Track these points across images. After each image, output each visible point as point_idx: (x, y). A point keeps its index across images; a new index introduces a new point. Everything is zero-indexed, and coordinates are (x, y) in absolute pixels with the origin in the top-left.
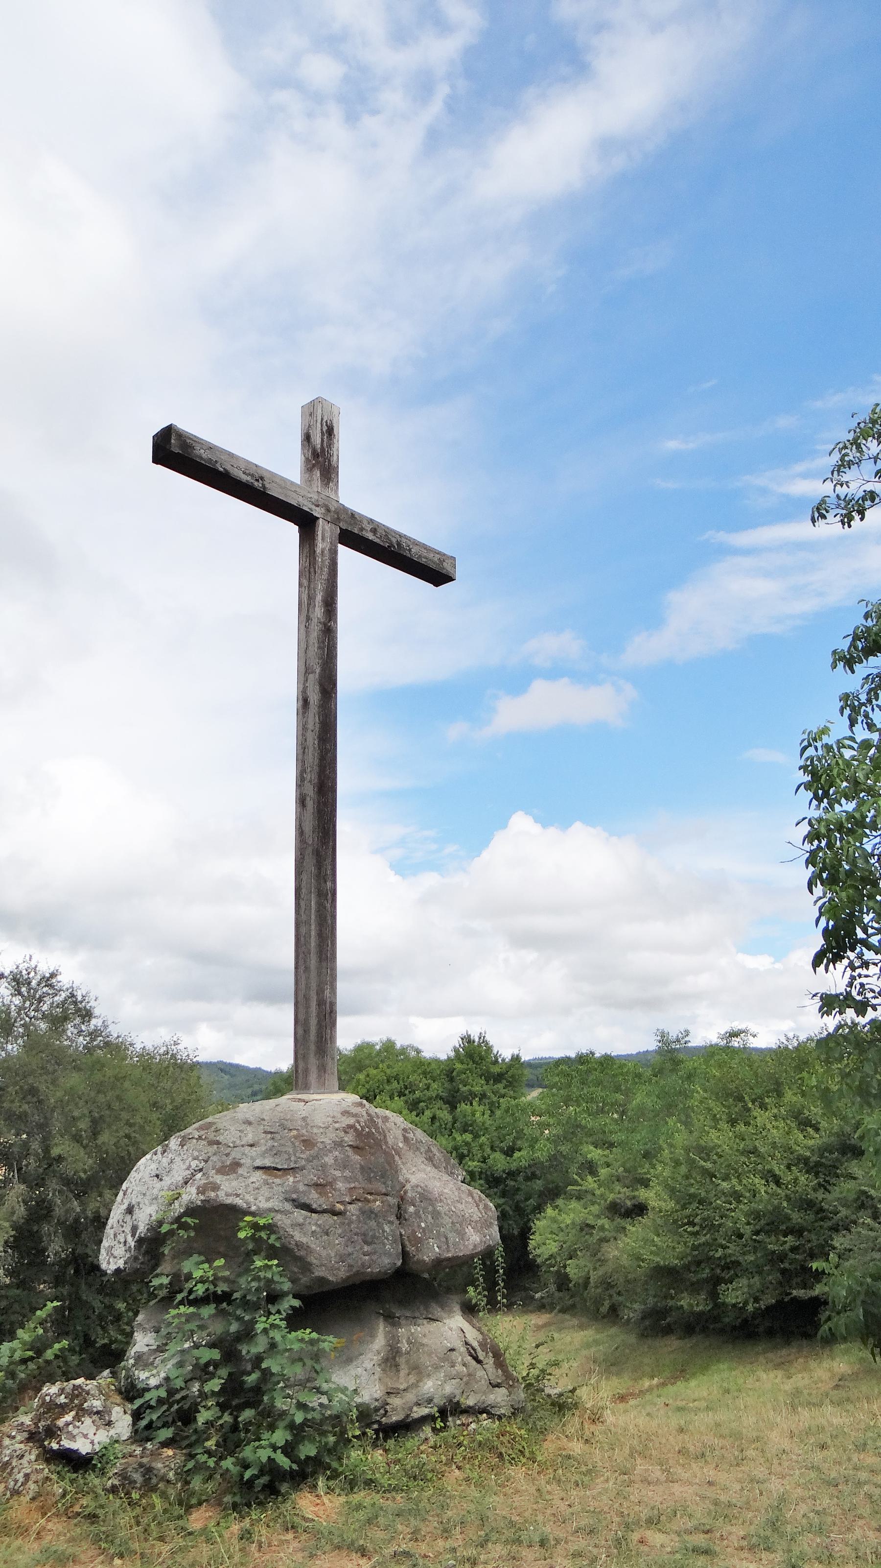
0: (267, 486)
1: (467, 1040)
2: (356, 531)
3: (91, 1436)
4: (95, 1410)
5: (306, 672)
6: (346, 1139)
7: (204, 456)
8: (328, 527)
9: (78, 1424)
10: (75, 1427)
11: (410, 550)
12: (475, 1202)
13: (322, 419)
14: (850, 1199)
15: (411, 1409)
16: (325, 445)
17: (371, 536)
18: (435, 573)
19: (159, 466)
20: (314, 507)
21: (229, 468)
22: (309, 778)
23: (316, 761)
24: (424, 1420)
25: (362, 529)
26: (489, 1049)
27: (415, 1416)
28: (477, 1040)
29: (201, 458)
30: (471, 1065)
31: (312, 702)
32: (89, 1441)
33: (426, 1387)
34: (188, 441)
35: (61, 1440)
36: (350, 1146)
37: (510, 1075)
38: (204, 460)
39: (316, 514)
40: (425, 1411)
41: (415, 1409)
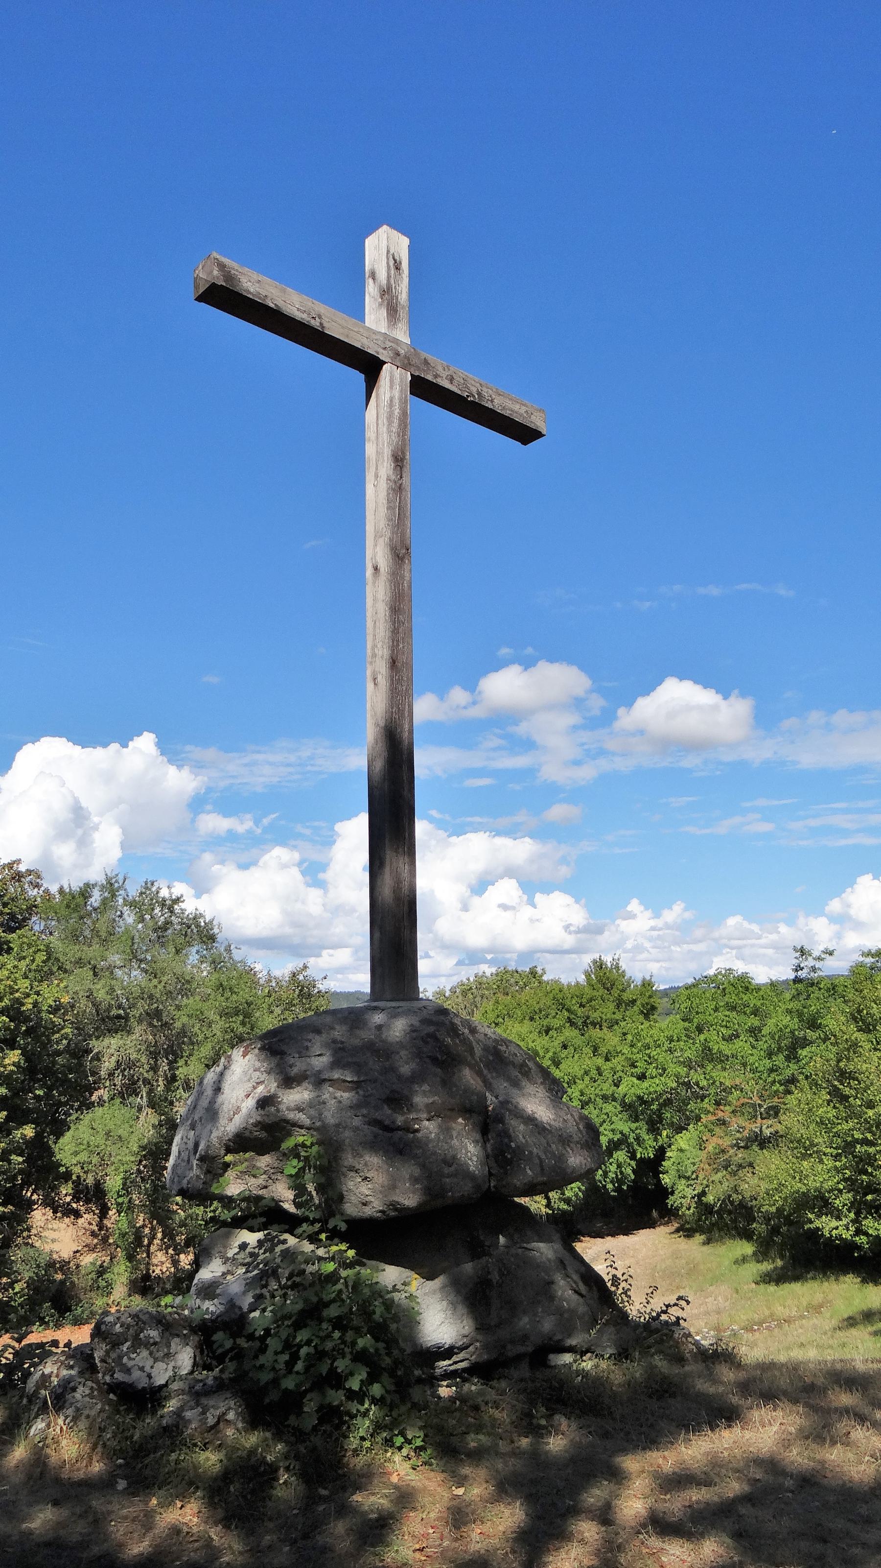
0: (325, 324)
1: (599, 965)
2: (429, 377)
3: (147, 1369)
4: (152, 1341)
5: (376, 536)
6: (425, 1049)
7: (252, 290)
8: (398, 372)
9: (133, 1356)
10: (130, 1359)
11: (492, 401)
12: (575, 1120)
13: (388, 252)
14: (616, 1382)
15: (504, 1347)
16: (392, 282)
17: (446, 384)
18: (525, 434)
19: (202, 304)
20: (381, 351)
21: (281, 304)
22: (380, 653)
23: (388, 634)
24: (519, 1358)
25: (436, 376)
26: (623, 974)
27: (510, 1354)
28: (609, 965)
29: (250, 293)
30: (602, 991)
31: (382, 570)
32: (145, 1374)
33: (521, 1323)
34: (233, 272)
35: (114, 1373)
36: (429, 1057)
37: (647, 1003)
38: (253, 295)
39: (382, 358)
40: (521, 1349)
41: (509, 1347)
